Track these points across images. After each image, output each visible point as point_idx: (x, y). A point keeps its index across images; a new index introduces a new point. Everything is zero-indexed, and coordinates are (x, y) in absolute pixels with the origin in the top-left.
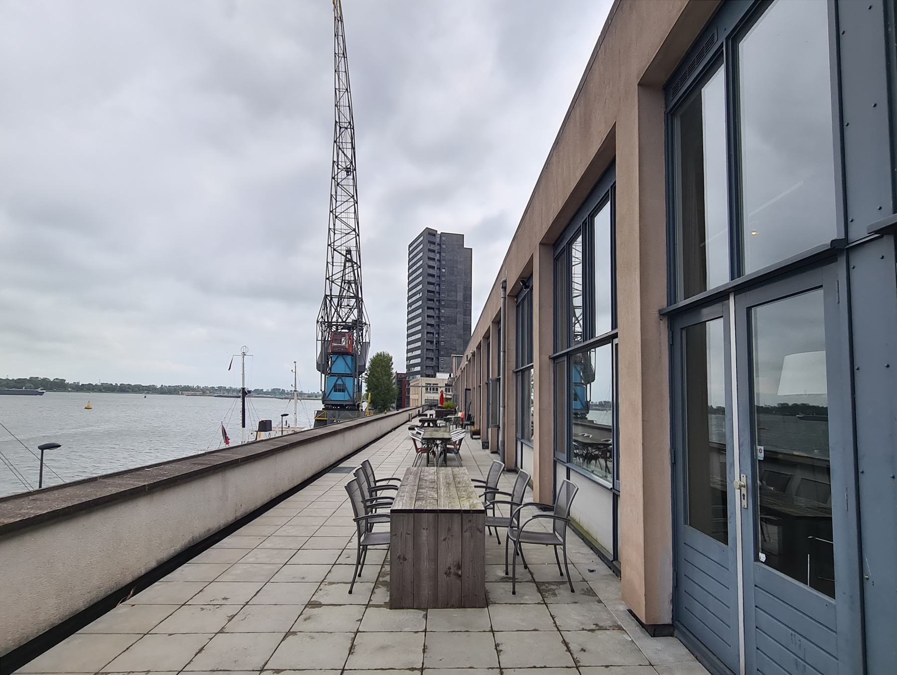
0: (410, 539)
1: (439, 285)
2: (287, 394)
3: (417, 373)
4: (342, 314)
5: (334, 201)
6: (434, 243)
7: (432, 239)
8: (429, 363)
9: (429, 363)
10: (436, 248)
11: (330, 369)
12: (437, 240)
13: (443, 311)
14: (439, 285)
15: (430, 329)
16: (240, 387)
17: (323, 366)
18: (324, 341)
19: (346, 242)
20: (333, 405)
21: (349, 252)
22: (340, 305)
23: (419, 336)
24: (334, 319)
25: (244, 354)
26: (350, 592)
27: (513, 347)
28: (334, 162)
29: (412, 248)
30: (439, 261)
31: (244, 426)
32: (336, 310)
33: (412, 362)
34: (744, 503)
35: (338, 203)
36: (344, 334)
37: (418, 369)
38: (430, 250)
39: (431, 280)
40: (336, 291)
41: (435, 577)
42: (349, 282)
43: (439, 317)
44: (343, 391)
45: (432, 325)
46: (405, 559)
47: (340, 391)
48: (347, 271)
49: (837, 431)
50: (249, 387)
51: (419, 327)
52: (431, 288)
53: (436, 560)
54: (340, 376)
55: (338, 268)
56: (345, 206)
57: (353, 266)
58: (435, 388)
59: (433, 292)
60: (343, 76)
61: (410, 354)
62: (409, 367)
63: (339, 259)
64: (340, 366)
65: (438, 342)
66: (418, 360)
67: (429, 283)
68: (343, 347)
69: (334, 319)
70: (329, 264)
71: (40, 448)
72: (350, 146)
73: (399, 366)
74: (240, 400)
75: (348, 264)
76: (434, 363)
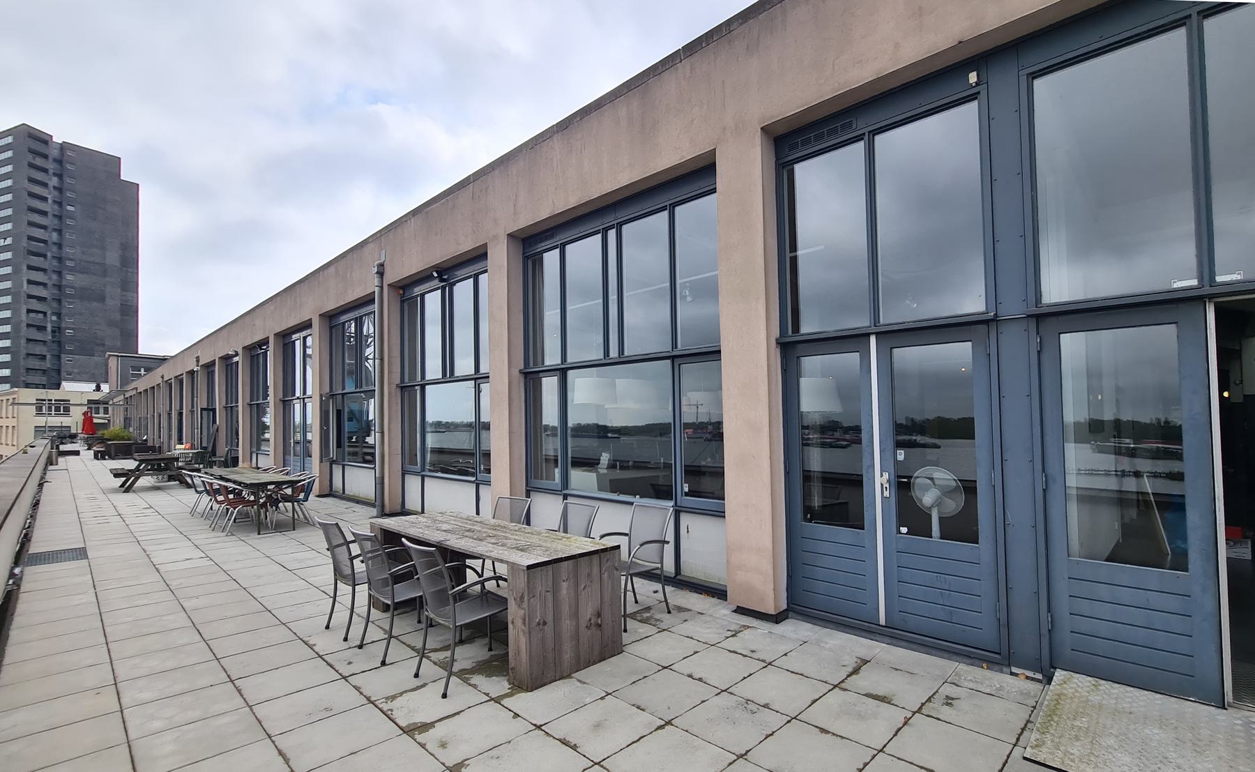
0: (549, 595)
6: (46, 157)
26: (444, 696)
27: (397, 353)
34: (887, 494)
41: (576, 637)
43: (59, 287)
46: (545, 623)
53: (576, 614)
65: (57, 330)
76: (47, 364)
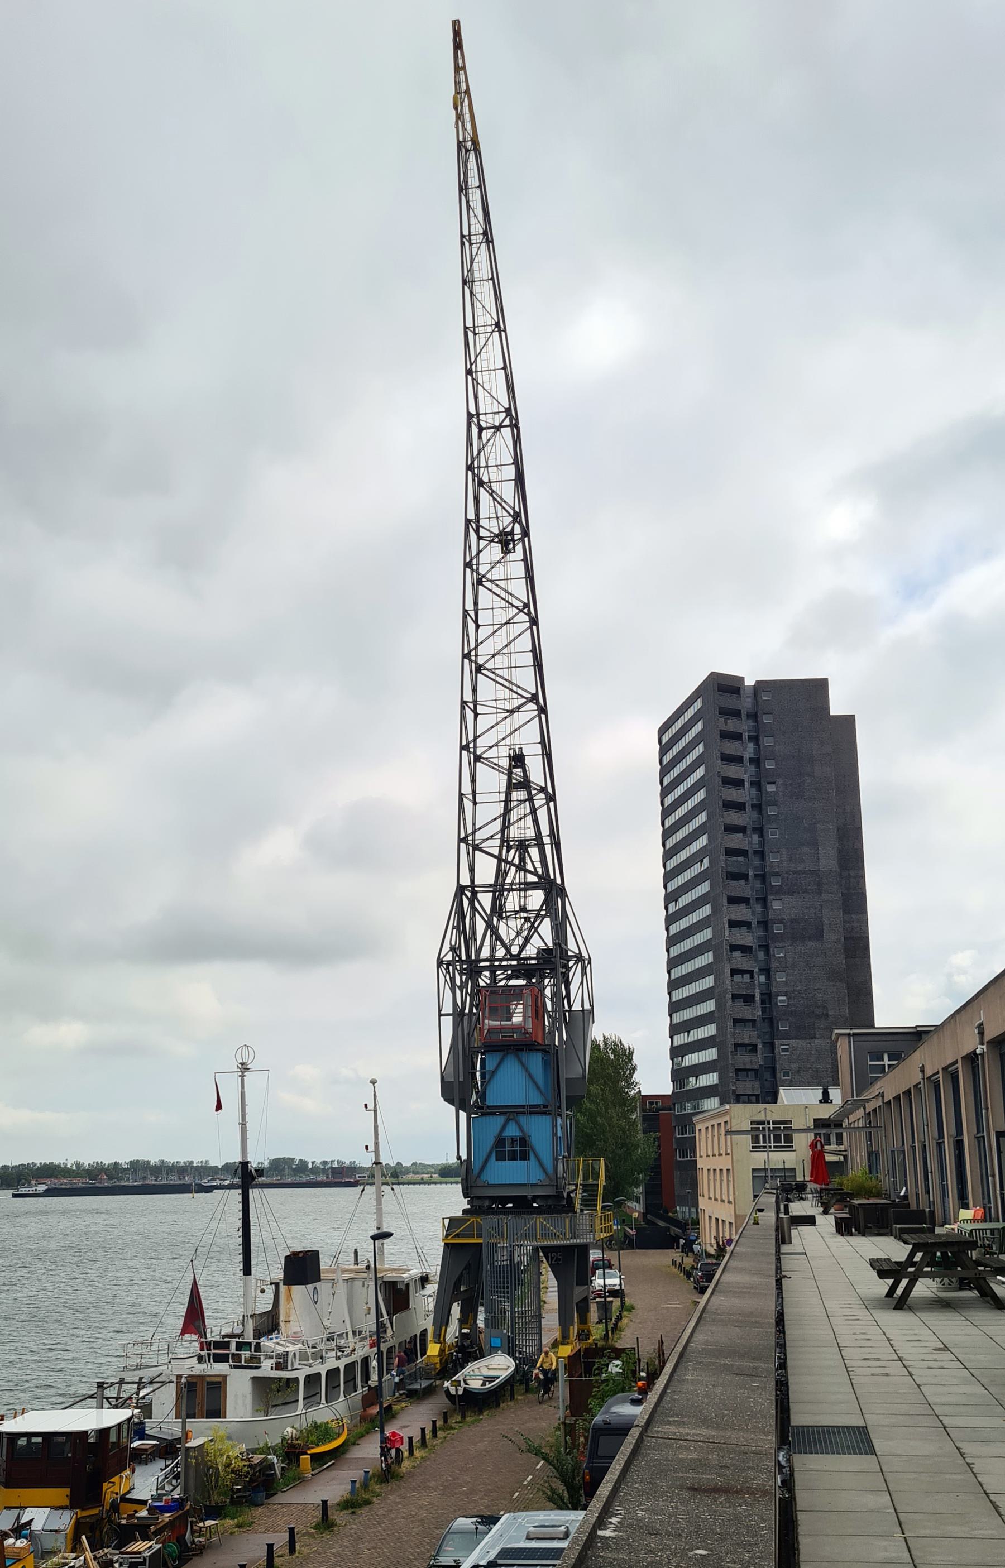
1: (760, 831)
2: (315, 1170)
3: (708, 1092)
4: (507, 930)
5: (471, 626)
6: (736, 714)
7: (730, 702)
8: (744, 1060)
9: (744, 1060)
10: (744, 726)
11: (482, 1096)
12: (746, 704)
13: (776, 905)
14: (760, 831)
15: (739, 960)
16: (237, 1158)
17: (457, 1089)
18: (458, 1015)
19: (495, 738)
20: (494, 1199)
21: (518, 759)
22: (498, 910)
23: (708, 982)
24: (485, 953)
25: (244, 1068)
28: (468, 522)
29: (670, 737)
30: (756, 761)
31: (247, 1270)
32: (489, 925)
33: (692, 1059)
35: (483, 633)
36: (516, 993)
37: (711, 1079)
38: (725, 735)
39: (735, 818)
40: (486, 871)
42: (522, 846)
44: (524, 1156)
45: (746, 950)
47: (513, 1157)
48: (514, 816)
49: (631, 1439)
50: (256, 1159)
51: (707, 958)
52: (736, 841)
54: (513, 1112)
55: (489, 811)
56: (501, 638)
57: (531, 799)
58: (781, 1134)
59: (744, 853)
60: (484, 291)
61: (681, 1039)
62: (679, 1076)
63: (492, 782)
64: (512, 1084)
65: (768, 998)
66: (710, 1054)
67: (729, 829)
68: (515, 1028)
69: (485, 953)
70: (466, 799)
71: (372, 1237)
72: (510, 472)
73: (653, 1077)
74: (236, 1194)
75: (518, 795)
76: (759, 1060)
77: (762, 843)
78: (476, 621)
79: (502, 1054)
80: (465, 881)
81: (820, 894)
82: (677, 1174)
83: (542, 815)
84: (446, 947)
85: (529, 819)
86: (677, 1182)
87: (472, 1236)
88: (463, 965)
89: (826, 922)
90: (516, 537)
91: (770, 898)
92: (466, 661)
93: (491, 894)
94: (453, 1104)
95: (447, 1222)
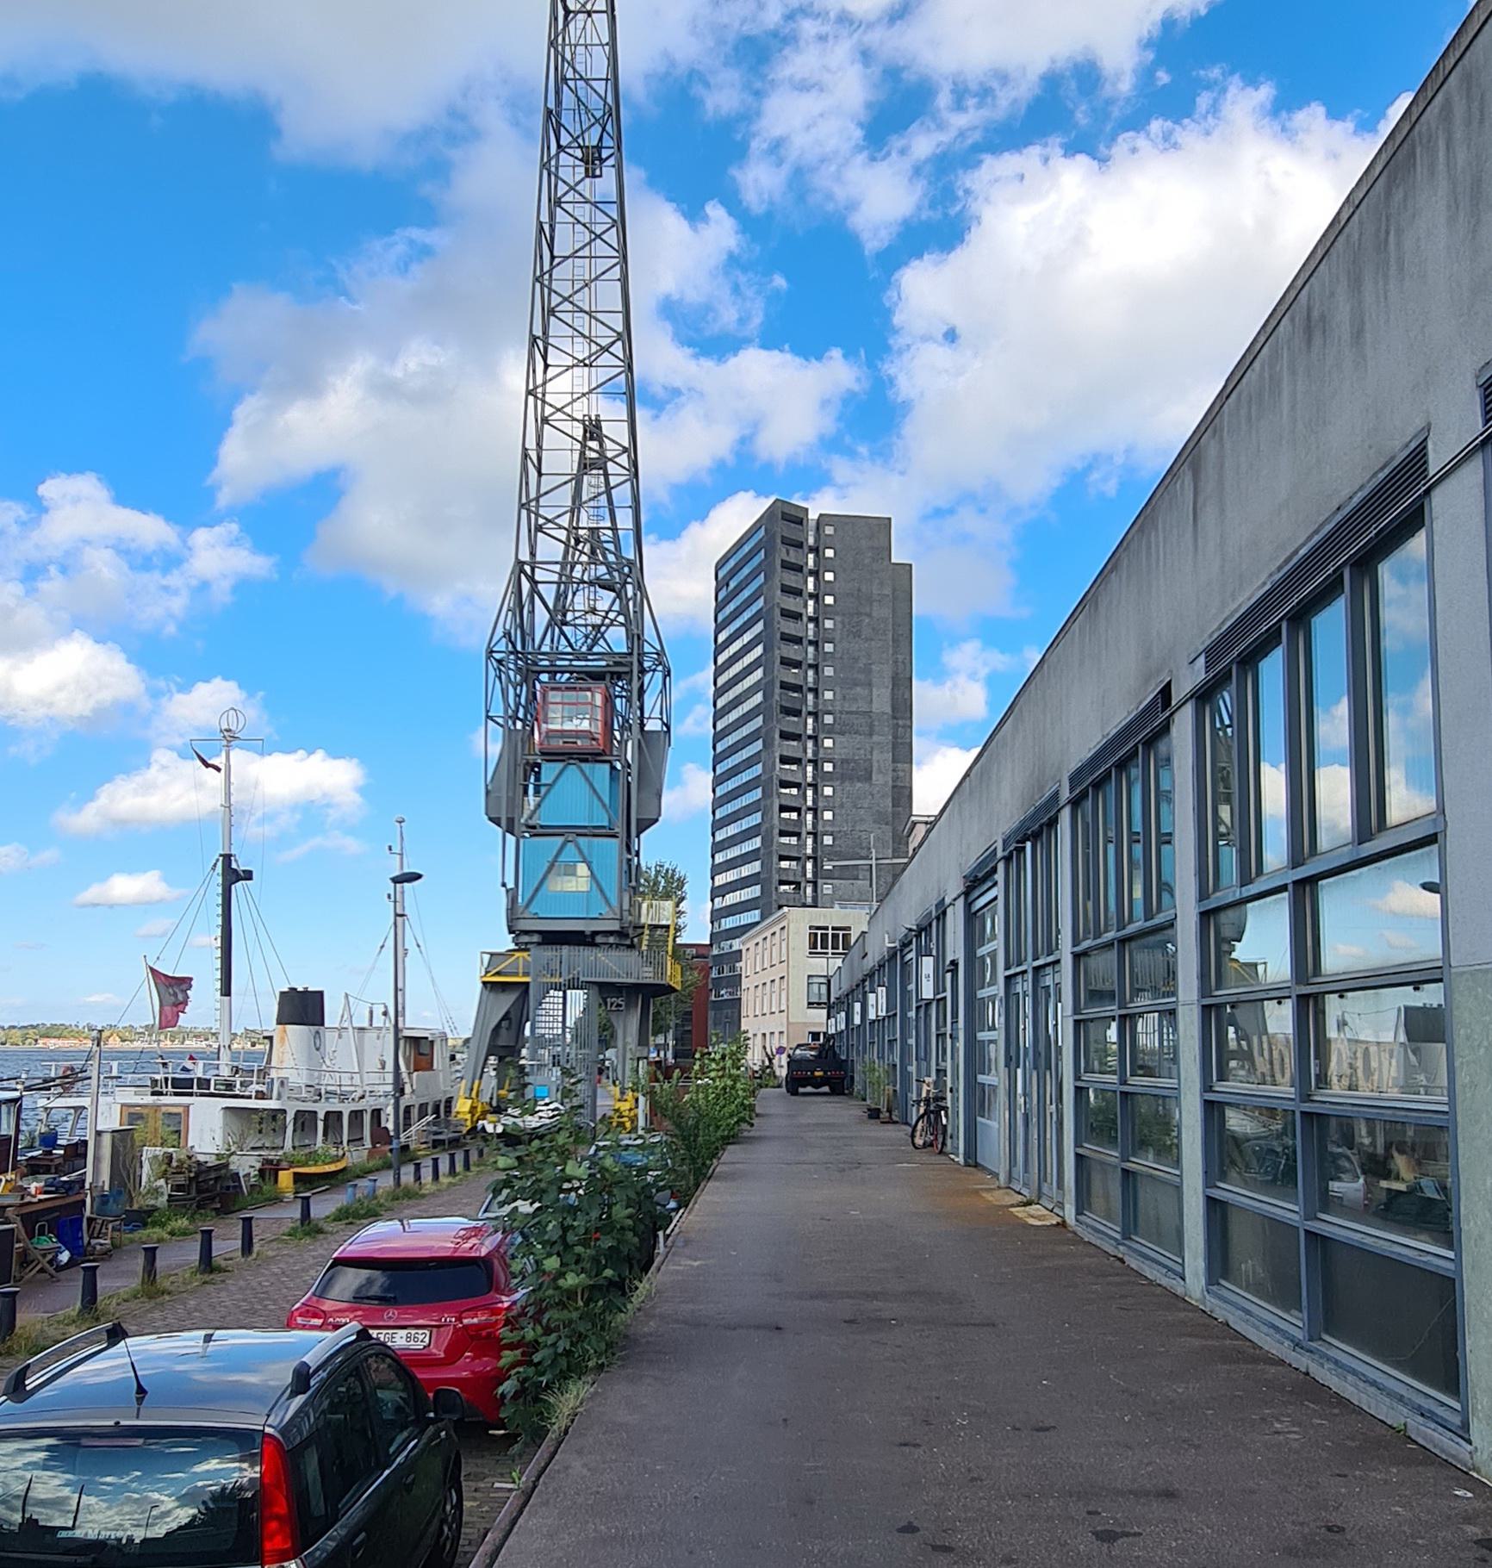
7: (791, 531)
13: (828, 743)
40: (550, 549)
70: (531, 460)
77: (816, 681)
78: (545, 358)
79: (560, 765)
80: (525, 556)
81: (871, 735)
82: (711, 1014)
83: (622, 495)
84: (500, 632)
85: (604, 497)
86: (710, 1022)
87: (516, 974)
88: (525, 667)
89: (875, 765)
90: (605, 154)
91: (821, 736)
92: (531, 399)
93: (555, 586)
94: (499, 825)
95: (486, 958)
